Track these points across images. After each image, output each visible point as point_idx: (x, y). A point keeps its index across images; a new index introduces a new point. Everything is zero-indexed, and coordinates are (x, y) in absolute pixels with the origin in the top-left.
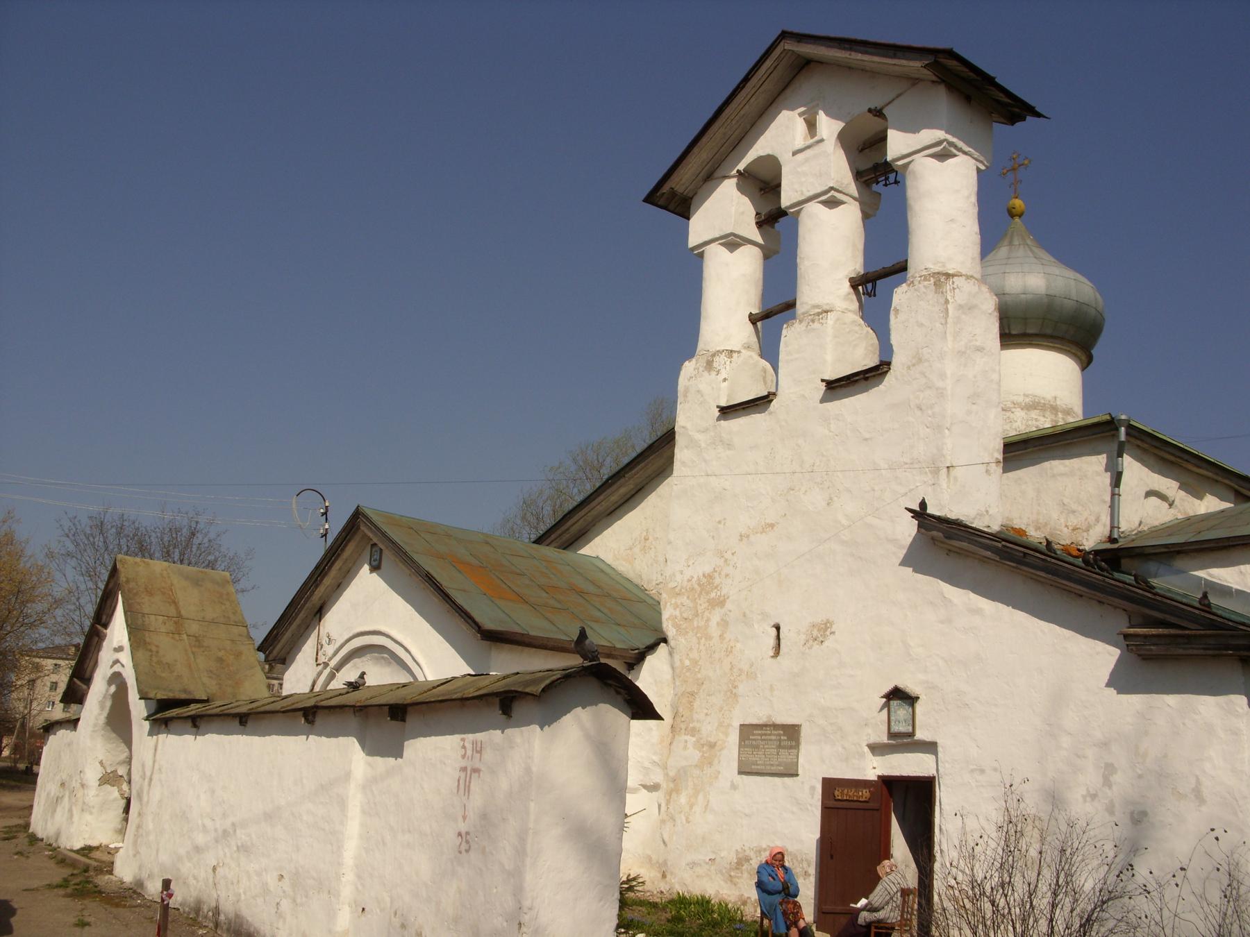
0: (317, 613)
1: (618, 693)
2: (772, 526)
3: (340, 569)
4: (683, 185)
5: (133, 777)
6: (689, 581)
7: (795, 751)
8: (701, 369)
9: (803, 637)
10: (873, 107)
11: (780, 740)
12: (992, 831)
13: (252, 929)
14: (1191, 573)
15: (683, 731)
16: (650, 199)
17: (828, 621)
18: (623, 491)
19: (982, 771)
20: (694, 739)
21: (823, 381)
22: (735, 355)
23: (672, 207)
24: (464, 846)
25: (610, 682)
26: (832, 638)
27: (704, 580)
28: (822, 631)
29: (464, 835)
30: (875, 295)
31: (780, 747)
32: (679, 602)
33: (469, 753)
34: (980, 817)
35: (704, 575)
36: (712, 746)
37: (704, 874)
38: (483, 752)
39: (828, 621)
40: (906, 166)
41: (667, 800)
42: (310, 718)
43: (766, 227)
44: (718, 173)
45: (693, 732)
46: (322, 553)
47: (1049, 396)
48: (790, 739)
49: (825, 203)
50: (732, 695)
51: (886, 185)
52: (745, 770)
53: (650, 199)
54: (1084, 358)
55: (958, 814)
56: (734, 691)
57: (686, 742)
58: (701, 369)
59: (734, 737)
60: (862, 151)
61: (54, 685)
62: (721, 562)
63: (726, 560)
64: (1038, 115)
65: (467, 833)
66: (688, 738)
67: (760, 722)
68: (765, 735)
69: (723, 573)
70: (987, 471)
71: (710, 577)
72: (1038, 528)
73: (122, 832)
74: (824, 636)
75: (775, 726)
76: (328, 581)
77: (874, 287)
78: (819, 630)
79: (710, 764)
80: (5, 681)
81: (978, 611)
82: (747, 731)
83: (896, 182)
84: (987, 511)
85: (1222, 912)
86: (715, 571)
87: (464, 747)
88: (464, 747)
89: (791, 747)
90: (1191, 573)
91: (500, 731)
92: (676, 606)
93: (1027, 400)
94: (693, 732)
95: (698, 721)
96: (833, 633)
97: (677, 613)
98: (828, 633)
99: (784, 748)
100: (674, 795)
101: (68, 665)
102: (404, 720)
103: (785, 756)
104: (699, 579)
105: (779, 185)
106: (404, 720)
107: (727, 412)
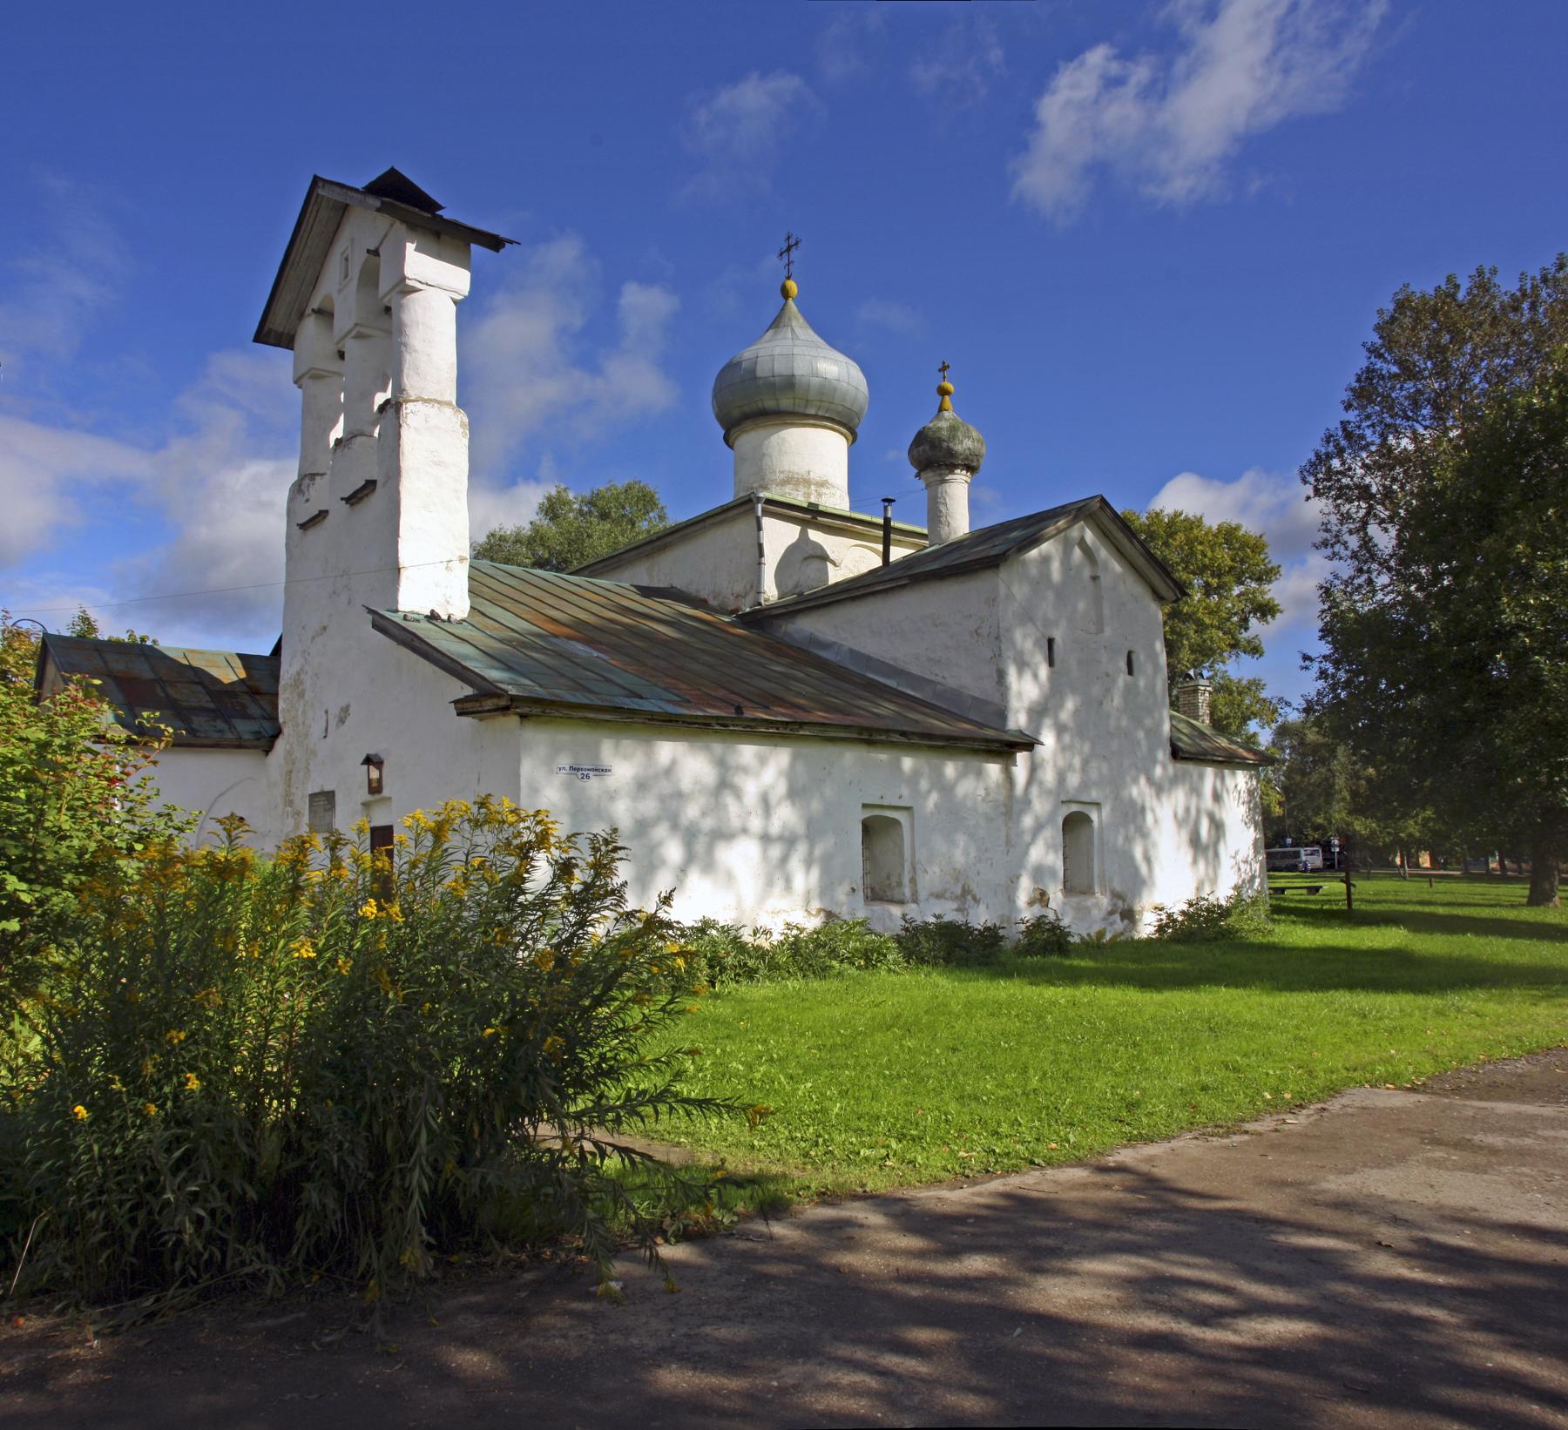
5: (728, 498)
12: (1267, 597)
13: (848, 405)
14: (342, 418)
16: (259, 338)
34: (176, 832)
37: (27, 1024)
40: (416, 290)
41: (576, 541)
49: (311, 377)
53: (259, 338)
54: (850, 438)
55: (336, 366)
61: (278, 323)
64: (511, 242)
72: (715, 598)
73: (340, 291)
80: (66, 941)
81: (297, 681)
85: (795, 1197)
90: (342, 418)
91: (916, 471)
101: (599, 1114)
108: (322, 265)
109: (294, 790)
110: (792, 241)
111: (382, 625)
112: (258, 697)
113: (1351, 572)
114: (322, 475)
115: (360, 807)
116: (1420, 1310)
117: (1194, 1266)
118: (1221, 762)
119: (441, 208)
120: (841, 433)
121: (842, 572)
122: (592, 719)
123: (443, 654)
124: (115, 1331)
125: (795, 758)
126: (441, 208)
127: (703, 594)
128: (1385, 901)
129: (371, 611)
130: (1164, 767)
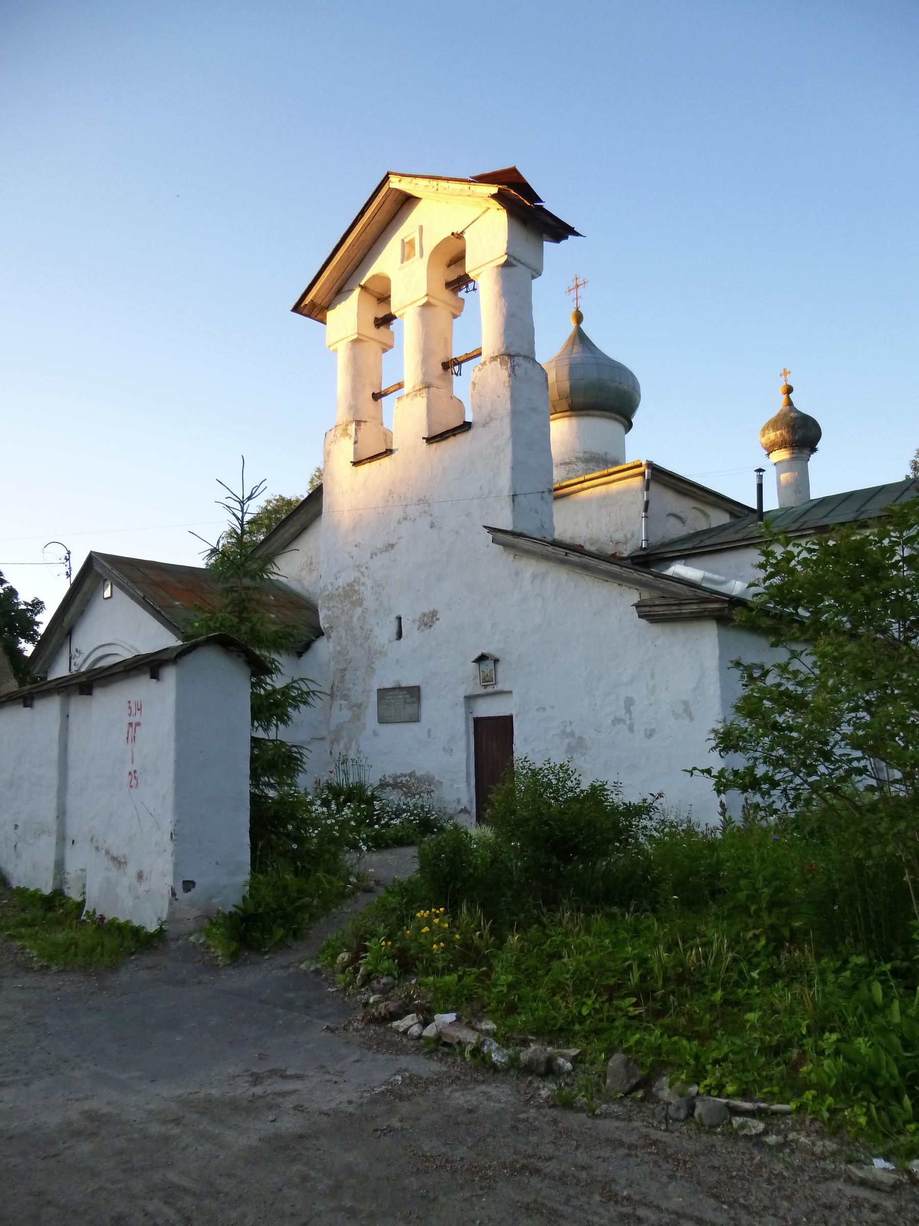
0: (67, 636)
1: (239, 656)
2: (392, 546)
3: (82, 600)
4: (320, 298)
6: (337, 589)
7: (416, 705)
8: (338, 436)
9: (417, 624)
10: (455, 232)
11: (405, 698)
15: (338, 698)
16: (297, 309)
17: (434, 611)
18: (292, 530)
19: (544, 709)
20: (347, 702)
21: (423, 438)
22: (362, 424)
23: (313, 315)
24: (134, 782)
25: (231, 648)
26: (437, 622)
27: (348, 588)
28: (429, 620)
29: (133, 773)
30: (460, 374)
31: (405, 702)
32: (331, 605)
33: (133, 711)
35: (347, 585)
36: (359, 706)
38: (143, 710)
39: (434, 611)
42: (29, 702)
43: (612, 454)
44: (346, 288)
45: (346, 697)
46: (68, 587)
47: (602, 452)
48: (412, 696)
50: (371, 669)
51: (467, 292)
52: (382, 720)
53: (297, 309)
56: (373, 666)
57: (341, 704)
58: (338, 436)
59: (374, 697)
60: (449, 266)
62: (358, 574)
63: (362, 573)
65: (135, 772)
66: (343, 702)
67: (391, 686)
68: (395, 695)
69: (360, 582)
70: (542, 498)
71: (351, 585)
72: (592, 544)
74: (433, 622)
75: (401, 689)
76: (73, 610)
77: (460, 369)
78: (428, 618)
79: (359, 719)
82: (383, 693)
83: (474, 289)
84: (543, 527)
86: (355, 581)
87: (130, 708)
88: (130, 708)
89: (413, 703)
92: (329, 609)
93: (586, 456)
94: (346, 697)
95: (349, 689)
96: (438, 619)
97: (330, 613)
98: (434, 619)
99: (408, 703)
100: (335, 744)
102: (90, 694)
103: (410, 710)
104: (344, 588)
105: (389, 297)
106: (90, 694)
107: (399, 619)
108: (609, 410)
109: (547, 1181)
110: (573, 293)
111: (388, 174)
112: (907, 1036)
113: (247, 565)
114: (366, 422)
115: (462, 700)
116: (34, 685)
117: (683, 488)
118: (309, 609)
119: (494, 196)
120: (616, 420)
121: (686, 528)
122: (108, 676)
123: (460, 433)
124: (793, 453)
125: (552, 535)
126: (494, 196)
127: (579, 541)
128: (419, 300)
129: (486, 527)
130: (807, 1099)
